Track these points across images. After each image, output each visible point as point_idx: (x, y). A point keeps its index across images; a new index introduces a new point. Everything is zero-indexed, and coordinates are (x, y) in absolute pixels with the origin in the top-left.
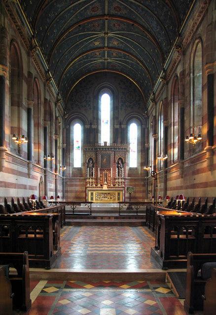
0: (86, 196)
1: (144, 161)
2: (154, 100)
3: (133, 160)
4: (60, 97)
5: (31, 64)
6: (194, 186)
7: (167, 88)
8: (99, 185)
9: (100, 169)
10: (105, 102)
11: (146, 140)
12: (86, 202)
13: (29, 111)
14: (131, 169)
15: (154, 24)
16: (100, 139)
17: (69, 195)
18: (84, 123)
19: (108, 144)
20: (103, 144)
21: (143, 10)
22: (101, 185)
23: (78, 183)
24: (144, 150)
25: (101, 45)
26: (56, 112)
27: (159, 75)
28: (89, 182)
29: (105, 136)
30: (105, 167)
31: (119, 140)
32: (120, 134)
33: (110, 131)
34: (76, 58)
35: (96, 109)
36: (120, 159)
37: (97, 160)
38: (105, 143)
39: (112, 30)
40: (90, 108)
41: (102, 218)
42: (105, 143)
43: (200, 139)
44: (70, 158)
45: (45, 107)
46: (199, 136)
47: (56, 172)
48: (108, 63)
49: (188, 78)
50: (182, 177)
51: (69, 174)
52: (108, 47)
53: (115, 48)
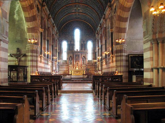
0: (69, 72)
1: (95, 58)
2: (97, 33)
3: (90, 57)
4: (58, 32)
5: (49, 24)
6: (109, 68)
7: (102, 30)
8: (74, 68)
9: (75, 61)
10: (77, 33)
11: (95, 48)
12: (69, 75)
13: (48, 41)
14: (89, 61)
15: (96, 7)
16: (75, 48)
17: (61, 72)
18: (68, 42)
19: (78, 50)
20: (76, 50)
21: (91, 3)
22: (76, 68)
23: (65, 67)
24: (94, 53)
25: (75, 12)
26: (56, 37)
27: (107, 5)
28: (70, 67)
29: (77, 47)
30: (77, 60)
31: (83, 49)
32: (83, 46)
33: (80, 45)
34: (64, 16)
35: (73, 35)
36: (84, 56)
37: (73, 57)
38: (77, 50)
39: (79, 7)
40: (70, 35)
41: (76, 80)
42: (77, 50)
43: (109, 52)
44: (61, 56)
45: (52, 37)
46: (109, 52)
47: (56, 62)
48: (78, 17)
49: (107, 30)
50: (106, 65)
51: (61, 63)
52: (78, 12)
53: (81, 13)
